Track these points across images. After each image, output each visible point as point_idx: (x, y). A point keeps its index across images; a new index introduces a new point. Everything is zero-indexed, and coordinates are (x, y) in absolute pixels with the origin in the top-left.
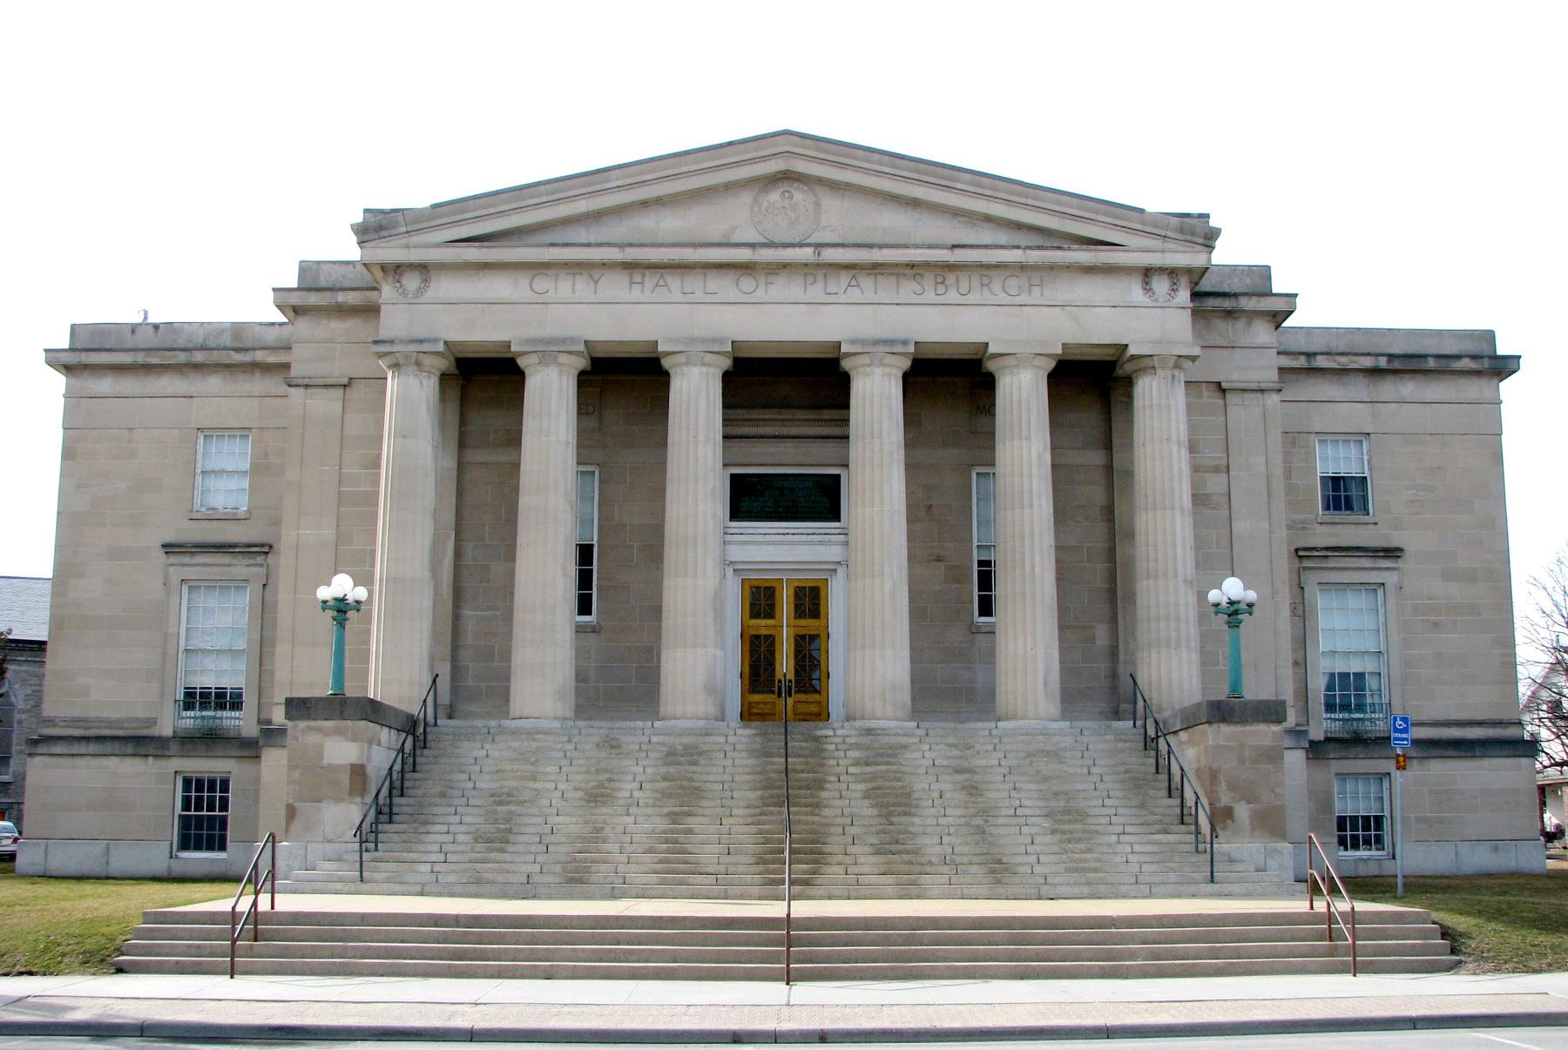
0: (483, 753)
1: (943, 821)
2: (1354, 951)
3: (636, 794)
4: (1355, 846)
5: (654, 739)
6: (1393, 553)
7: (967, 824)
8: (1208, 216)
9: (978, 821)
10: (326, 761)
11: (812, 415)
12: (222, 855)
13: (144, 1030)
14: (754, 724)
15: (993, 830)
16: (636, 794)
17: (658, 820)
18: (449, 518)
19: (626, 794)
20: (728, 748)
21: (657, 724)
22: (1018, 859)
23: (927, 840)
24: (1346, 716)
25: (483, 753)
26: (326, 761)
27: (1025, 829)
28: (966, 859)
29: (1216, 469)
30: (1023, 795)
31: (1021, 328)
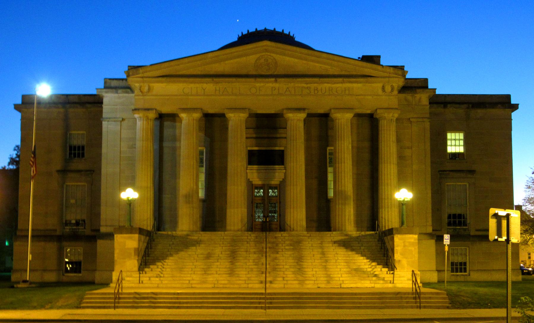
0: (171, 243)
1: (314, 264)
2: (420, 303)
3: (220, 255)
4: (457, 272)
5: (225, 238)
6: (472, 172)
7: (321, 265)
8: (404, 66)
9: (324, 264)
10: (126, 247)
11: (156, 319)
12: (80, 275)
13: (85, 321)
14: (256, 233)
15: (329, 267)
16: (220, 255)
17: (227, 264)
18: (158, 162)
19: (217, 255)
20: (248, 240)
21: (226, 233)
22: (335, 276)
23: (309, 270)
24: (454, 227)
25: (171, 243)
26: (126, 247)
27: (314, 270)
28: (320, 276)
29: (408, 148)
30: (339, 256)
31: (345, 100)
